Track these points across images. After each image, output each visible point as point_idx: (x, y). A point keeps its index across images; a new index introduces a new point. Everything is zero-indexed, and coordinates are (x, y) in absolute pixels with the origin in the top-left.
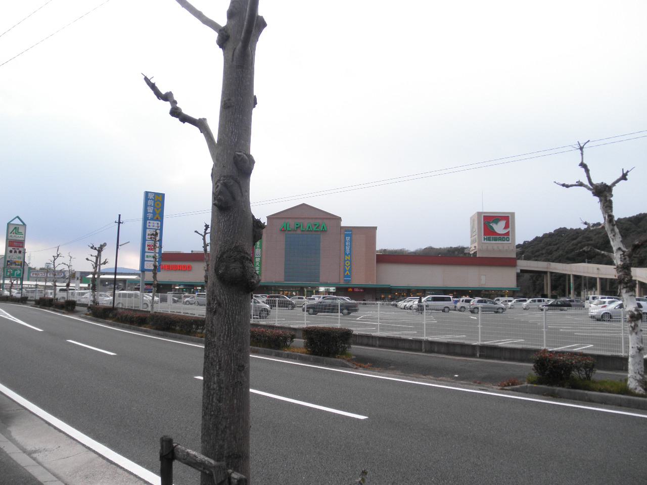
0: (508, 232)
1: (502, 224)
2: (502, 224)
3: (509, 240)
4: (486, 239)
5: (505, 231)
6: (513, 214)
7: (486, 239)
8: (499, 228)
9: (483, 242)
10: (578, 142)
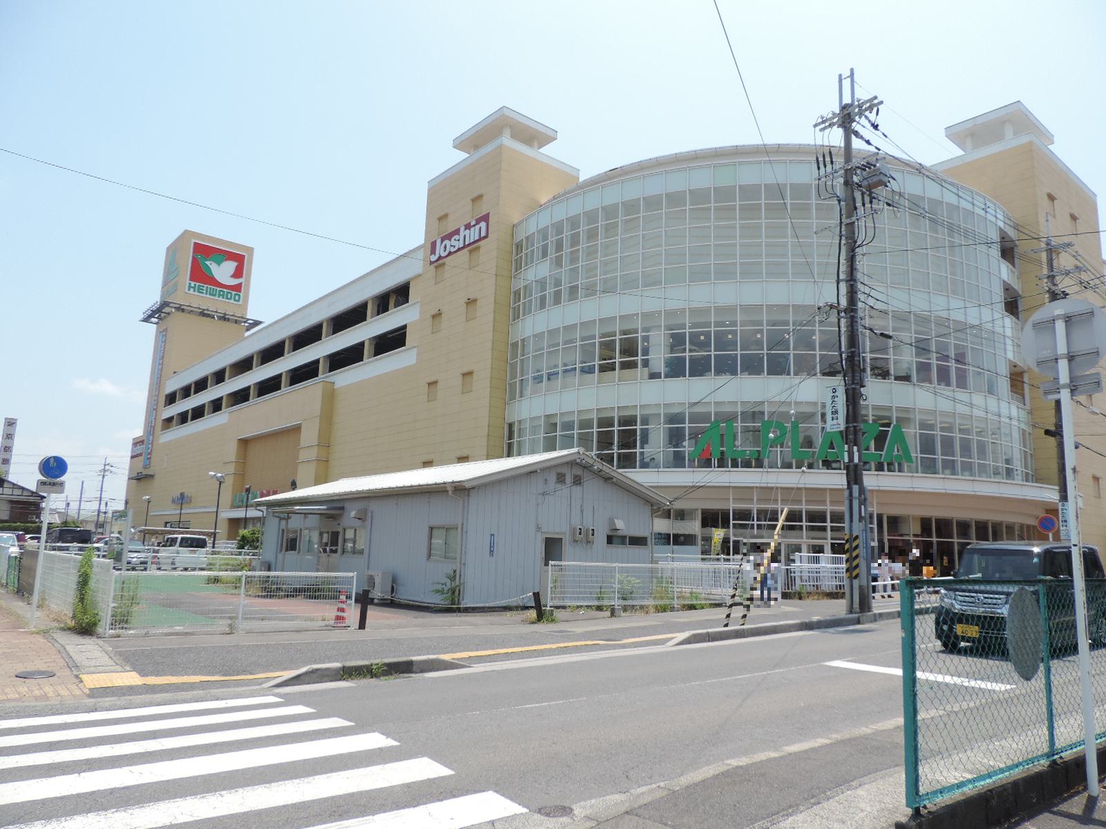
0: (240, 285)
1: (231, 266)
2: (231, 266)
3: (238, 301)
4: (194, 288)
5: (235, 282)
6: (250, 250)
7: (194, 288)
8: (223, 272)
9: (187, 291)
10: (852, 70)
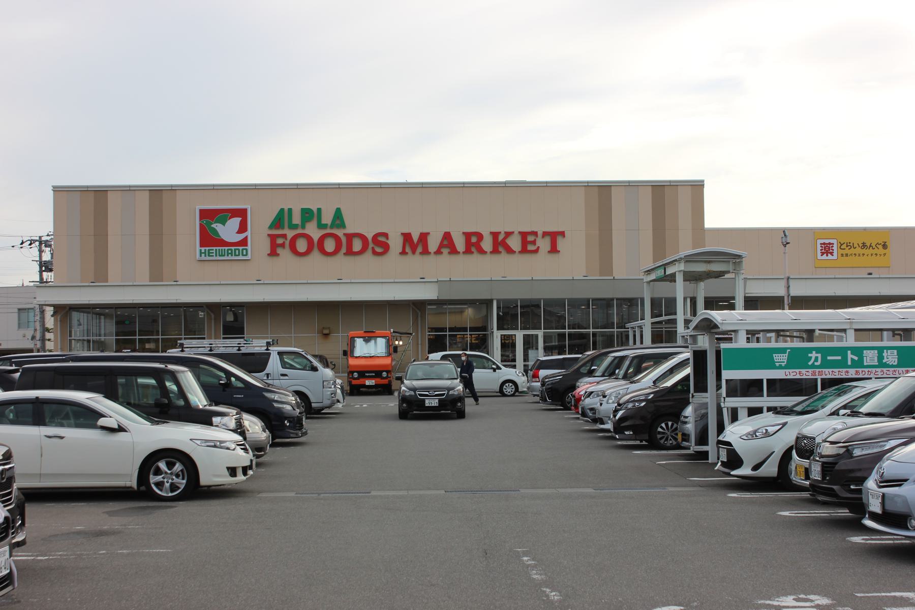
5: (241, 237)
